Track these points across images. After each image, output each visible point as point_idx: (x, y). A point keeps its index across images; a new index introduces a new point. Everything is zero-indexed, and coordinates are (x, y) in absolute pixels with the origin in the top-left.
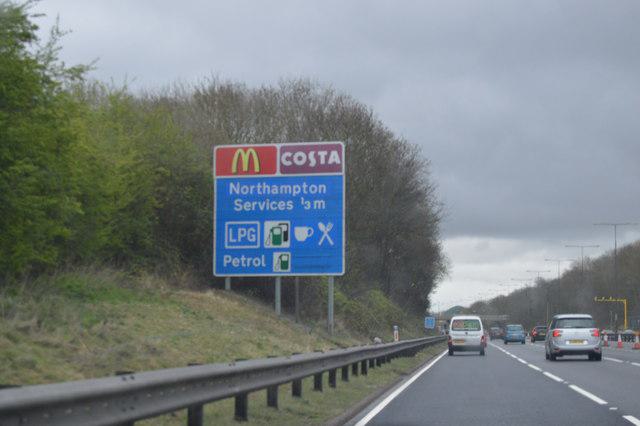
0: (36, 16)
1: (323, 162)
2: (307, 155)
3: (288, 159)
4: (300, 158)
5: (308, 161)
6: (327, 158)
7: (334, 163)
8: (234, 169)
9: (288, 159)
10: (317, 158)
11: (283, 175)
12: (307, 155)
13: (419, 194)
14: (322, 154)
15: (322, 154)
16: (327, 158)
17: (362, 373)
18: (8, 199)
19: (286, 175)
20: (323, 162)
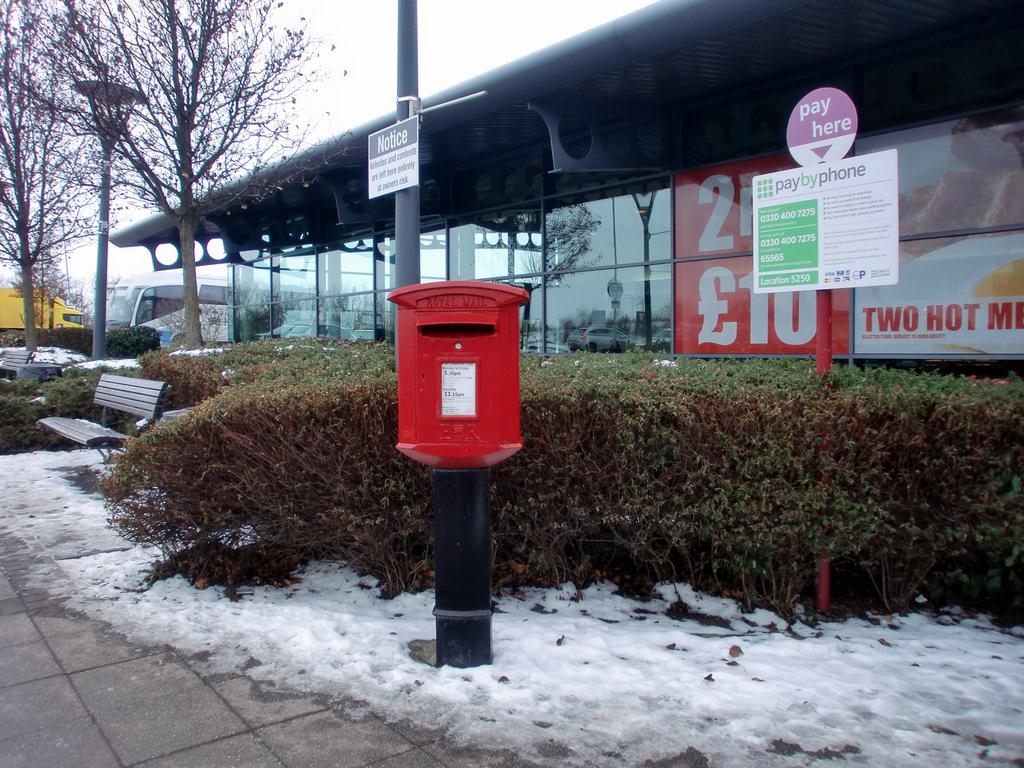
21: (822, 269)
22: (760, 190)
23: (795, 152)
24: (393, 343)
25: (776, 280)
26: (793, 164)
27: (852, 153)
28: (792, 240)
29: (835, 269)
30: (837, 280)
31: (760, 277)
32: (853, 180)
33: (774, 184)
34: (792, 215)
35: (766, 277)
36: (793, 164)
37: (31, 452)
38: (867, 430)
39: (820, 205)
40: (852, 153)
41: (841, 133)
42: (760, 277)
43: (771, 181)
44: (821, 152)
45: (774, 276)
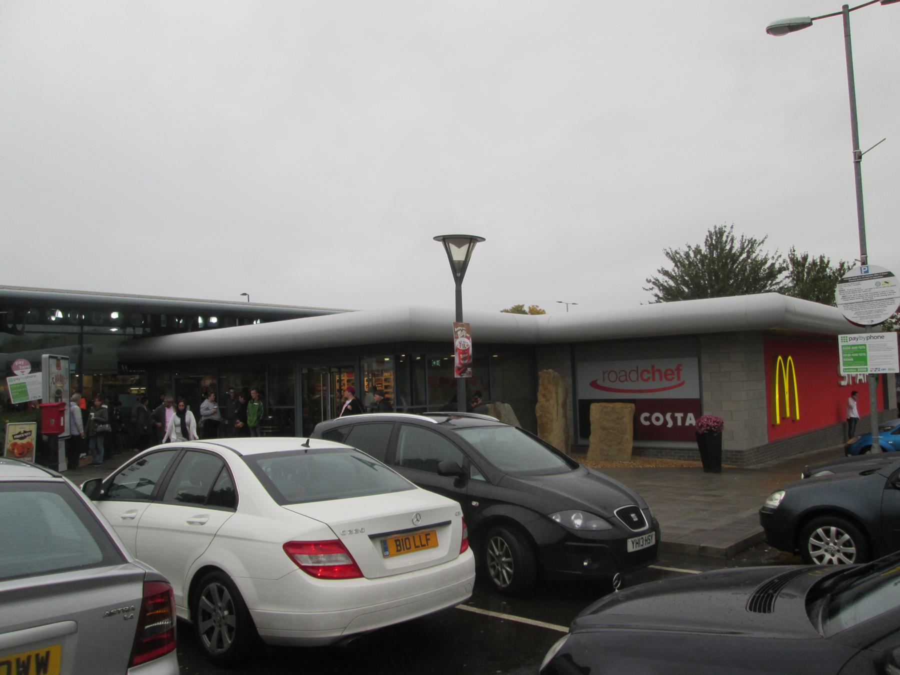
0: (652, 289)
1: (679, 423)
2: (664, 416)
3: (646, 419)
4: (658, 419)
5: (666, 422)
6: (684, 419)
7: (691, 425)
8: (845, 355)
9: (646, 419)
10: (674, 419)
11: (505, 542)
12: (664, 416)
13: (169, 590)
14: (679, 416)
15: (679, 416)
16: (684, 419)
17: (768, 610)
18: (676, 269)
19: (234, 611)
20: (679, 423)
21: (869, 367)
22: (844, 337)
23: (16, 372)
24: (331, 398)
25: (850, 370)
26: (15, 375)
27: (30, 373)
28: (856, 355)
29: (874, 367)
30: (875, 371)
31: (844, 369)
32: (879, 339)
33: (848, 338)
34: (15, 386)
35: (846, 369)
36: (15, 375)
37: (66, 456)
38: (715, 430)
39: (867, 346)
40: (30, 373)
41: (27, 368)
42: (844, 369)
43: (847, 337)
44: (23, 372)
45: (850, 369)
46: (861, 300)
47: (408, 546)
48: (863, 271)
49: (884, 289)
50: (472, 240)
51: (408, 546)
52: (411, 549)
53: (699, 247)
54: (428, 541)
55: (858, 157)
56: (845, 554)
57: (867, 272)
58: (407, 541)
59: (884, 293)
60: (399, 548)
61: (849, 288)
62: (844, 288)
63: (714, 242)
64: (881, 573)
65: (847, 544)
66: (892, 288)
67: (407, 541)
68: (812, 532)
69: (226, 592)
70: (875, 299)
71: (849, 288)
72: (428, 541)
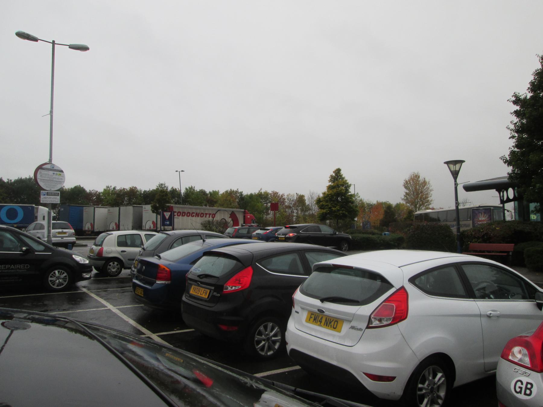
46: (48, 179)
47: (335, 326)
48: (52, 167)
49: (58, 177)
50: (461, 162)
51: (335, 326)
52: (336, 330)
53: (329, 181)
54: (311, 318)
55: (51, 112)
56: (266, 330)
57: (53, 168)
58: (336, 323)
59: (58, 179)
60: (529, 386)
61: (44, 172)
62: (42, 172)
63: (425, 193)
64: (110, 285)
65: (266, 328)
66: (61, 177)
67: (336, 323)
68: (267, 322)
69: (119, 270)
70: (55, 180)
71: (44, 172)
72: (311, 318)
